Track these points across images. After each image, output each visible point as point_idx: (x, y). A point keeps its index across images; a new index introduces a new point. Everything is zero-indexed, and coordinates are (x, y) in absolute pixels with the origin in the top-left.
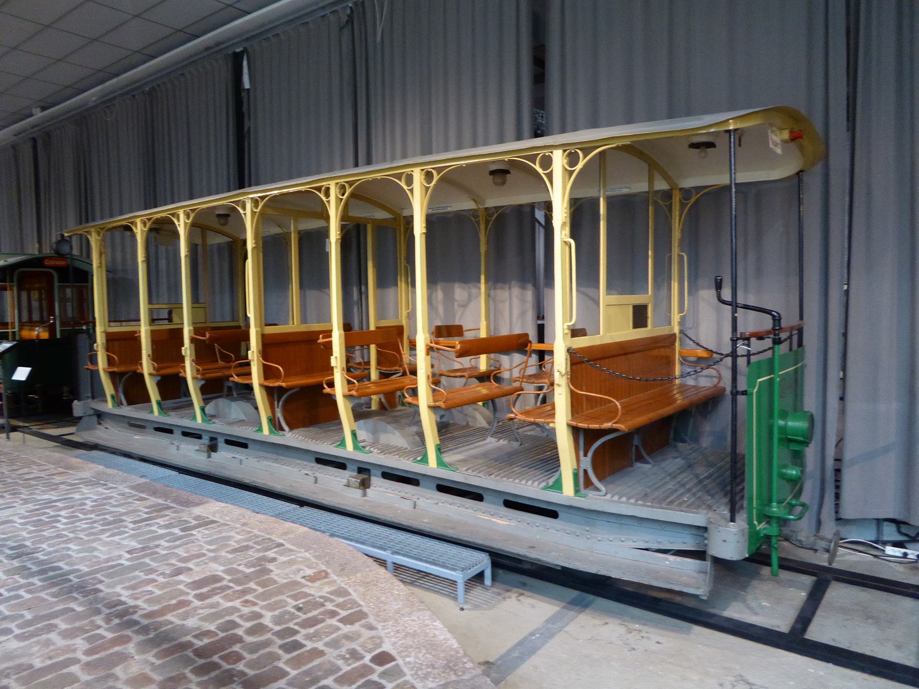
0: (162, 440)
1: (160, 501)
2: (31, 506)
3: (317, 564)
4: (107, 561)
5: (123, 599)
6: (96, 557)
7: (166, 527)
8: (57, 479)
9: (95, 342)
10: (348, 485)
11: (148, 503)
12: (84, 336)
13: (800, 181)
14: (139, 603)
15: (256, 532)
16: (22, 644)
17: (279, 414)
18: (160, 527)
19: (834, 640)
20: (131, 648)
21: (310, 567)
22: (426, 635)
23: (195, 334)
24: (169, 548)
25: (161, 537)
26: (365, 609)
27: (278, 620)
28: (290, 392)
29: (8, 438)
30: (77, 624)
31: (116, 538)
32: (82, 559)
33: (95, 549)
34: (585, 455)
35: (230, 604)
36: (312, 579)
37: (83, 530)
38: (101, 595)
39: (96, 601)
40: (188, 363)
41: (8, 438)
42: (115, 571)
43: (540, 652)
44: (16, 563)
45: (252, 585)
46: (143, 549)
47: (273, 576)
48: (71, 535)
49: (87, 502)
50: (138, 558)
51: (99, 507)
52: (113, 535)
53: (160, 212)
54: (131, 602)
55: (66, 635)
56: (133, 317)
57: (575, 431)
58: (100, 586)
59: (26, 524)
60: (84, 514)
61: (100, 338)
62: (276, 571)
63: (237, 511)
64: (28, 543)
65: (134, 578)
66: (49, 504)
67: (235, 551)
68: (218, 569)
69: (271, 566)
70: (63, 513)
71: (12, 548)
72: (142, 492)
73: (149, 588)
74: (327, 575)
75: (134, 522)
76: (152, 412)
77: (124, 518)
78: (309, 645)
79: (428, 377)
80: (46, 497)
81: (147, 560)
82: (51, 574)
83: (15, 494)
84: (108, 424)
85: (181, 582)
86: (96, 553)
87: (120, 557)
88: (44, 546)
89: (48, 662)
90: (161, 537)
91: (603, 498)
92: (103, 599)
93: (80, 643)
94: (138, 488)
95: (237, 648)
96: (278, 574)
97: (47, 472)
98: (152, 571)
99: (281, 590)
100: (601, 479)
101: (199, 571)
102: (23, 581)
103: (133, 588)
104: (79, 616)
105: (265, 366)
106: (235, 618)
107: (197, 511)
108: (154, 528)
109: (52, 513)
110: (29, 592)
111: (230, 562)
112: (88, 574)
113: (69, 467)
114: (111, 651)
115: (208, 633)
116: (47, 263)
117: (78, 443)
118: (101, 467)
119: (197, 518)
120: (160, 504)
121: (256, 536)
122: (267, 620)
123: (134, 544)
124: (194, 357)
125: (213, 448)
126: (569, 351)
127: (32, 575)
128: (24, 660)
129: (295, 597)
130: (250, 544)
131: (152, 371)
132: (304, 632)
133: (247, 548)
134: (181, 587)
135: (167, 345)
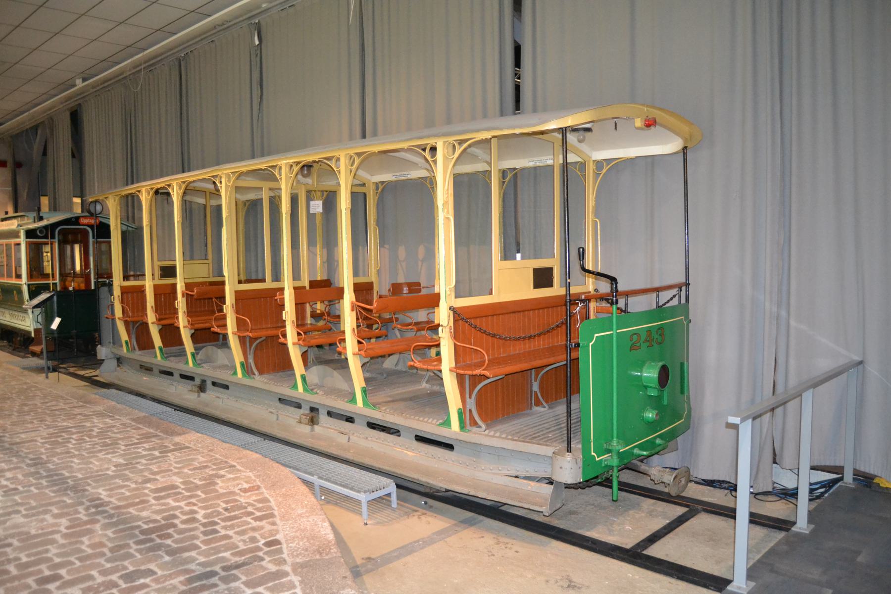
0: (164, 381)
1: (152, 431)
2: (51, 430)
3: (255, 481)
4: (97, 471)
5: (102, 497)
6: (90, 468)
7: (150, 449)
8: (77, 411)
9: (224, 303)
10: (300, 422)
11: (141, 432)
12: (106, 289)
13: (685, 154)
14: (112, 500)
15: (217, 456)
16: (26, 520)
17: (251, 361)
18: (145, 450)
19: (119, 379)
20: (97, 527)
21: (247, 482)
22: (313, 530)
23: (186, 289)
24: (146, 465)
25: (143, 457)
26: (276, 513)
27: (206, 516)
28: (258, 341)
29: (47, 377)
30: (65, 510)
31: (109, 456)
32: (79, 470)
33: (91, 463)
34: (470, 397)
35: (177, 504)
36: (245, 491)
37: (86, 449)
38: (87, 493)
39: (83, 496)
40: (181, 315)
41: (47, 377)
42: (101, 478)
43: (415, 554)
44: (32, 470)
45: (199, 493)
46: (127, 464)
47: (217, 487)
48: (77, 453)
49: (95, 429)
50: (120, 471)
51: (102, 434)
52: (107, 454)
53: (160, 183)
54: (107, 499)
55: (56, 516)
56: (260, 277)
57: (460, 379)
58: (87, 488)
59: (46, 443)
60: (90, 438)
61: (117, 292)
62: (221, 484)
63: (209, 440)
64: (44, 457)
65: (114, 483)
66: (65, 430)
67: (194, 469)
68: (177, 480)
69: (218, 481)
70: (74, 436)
71: (31, 460)
72: (140, 423)
73: (123, 491)
74: (259, 488)
75: (126, 446)
76: (156, 356)
77: (120, 442)
78: (223, 532)
79: (354, 330)
80: (65, 424)
81: (127, 472)
82: (55, 478)
83: (42, 421)
84: (125, 368)
85: (147, 488)
86: (91, 466)
87: (108, 469)
88: (55, 459)
89: (40, 532)
90: (143, 457)
91: (482, 435)
92: (87, 496)
93: (64, 522)
94: (137, 420)
95: (171, 531)
96: (221, 486)
97: (71, 405)
98: (129, 479)
99: (219, 496)
100: (484, 420)
101: (162, 481)
102: (34, 481)
103: (111, 490)
104: (68, 506)
105: (237, 319)
106: (177, 513)
107: (177, 439)
108: (140, 450)
109: (66, 436)
110: (37, 488)
111: (189, 476)
112: (81, 479)
113: (89, 402)
114: (84, 527)
115: (155, 521)
116: (83, 221)
117: (103, 383)
118: (114, 403)
119: (175, 444)
120: (151, 433)
121: (216, 459)
122: (199, 516)
123: (122, 461)
124: (185, 309)
125: (202, 388)
126: (122, 288)
127: (42, 478)
128: (25, 529)
129: (227, 502)
130: (210, 464)
131: (186, 324)
132: (223, 524)
133: (207, 467)
134: (146, 491)
135: (166, 296)
